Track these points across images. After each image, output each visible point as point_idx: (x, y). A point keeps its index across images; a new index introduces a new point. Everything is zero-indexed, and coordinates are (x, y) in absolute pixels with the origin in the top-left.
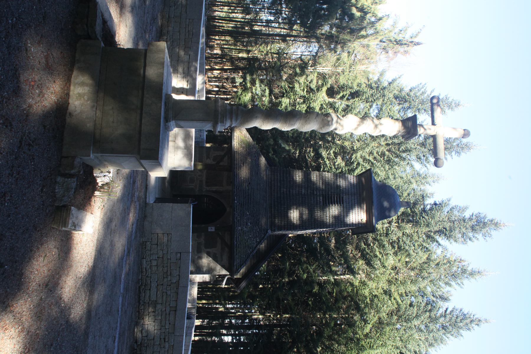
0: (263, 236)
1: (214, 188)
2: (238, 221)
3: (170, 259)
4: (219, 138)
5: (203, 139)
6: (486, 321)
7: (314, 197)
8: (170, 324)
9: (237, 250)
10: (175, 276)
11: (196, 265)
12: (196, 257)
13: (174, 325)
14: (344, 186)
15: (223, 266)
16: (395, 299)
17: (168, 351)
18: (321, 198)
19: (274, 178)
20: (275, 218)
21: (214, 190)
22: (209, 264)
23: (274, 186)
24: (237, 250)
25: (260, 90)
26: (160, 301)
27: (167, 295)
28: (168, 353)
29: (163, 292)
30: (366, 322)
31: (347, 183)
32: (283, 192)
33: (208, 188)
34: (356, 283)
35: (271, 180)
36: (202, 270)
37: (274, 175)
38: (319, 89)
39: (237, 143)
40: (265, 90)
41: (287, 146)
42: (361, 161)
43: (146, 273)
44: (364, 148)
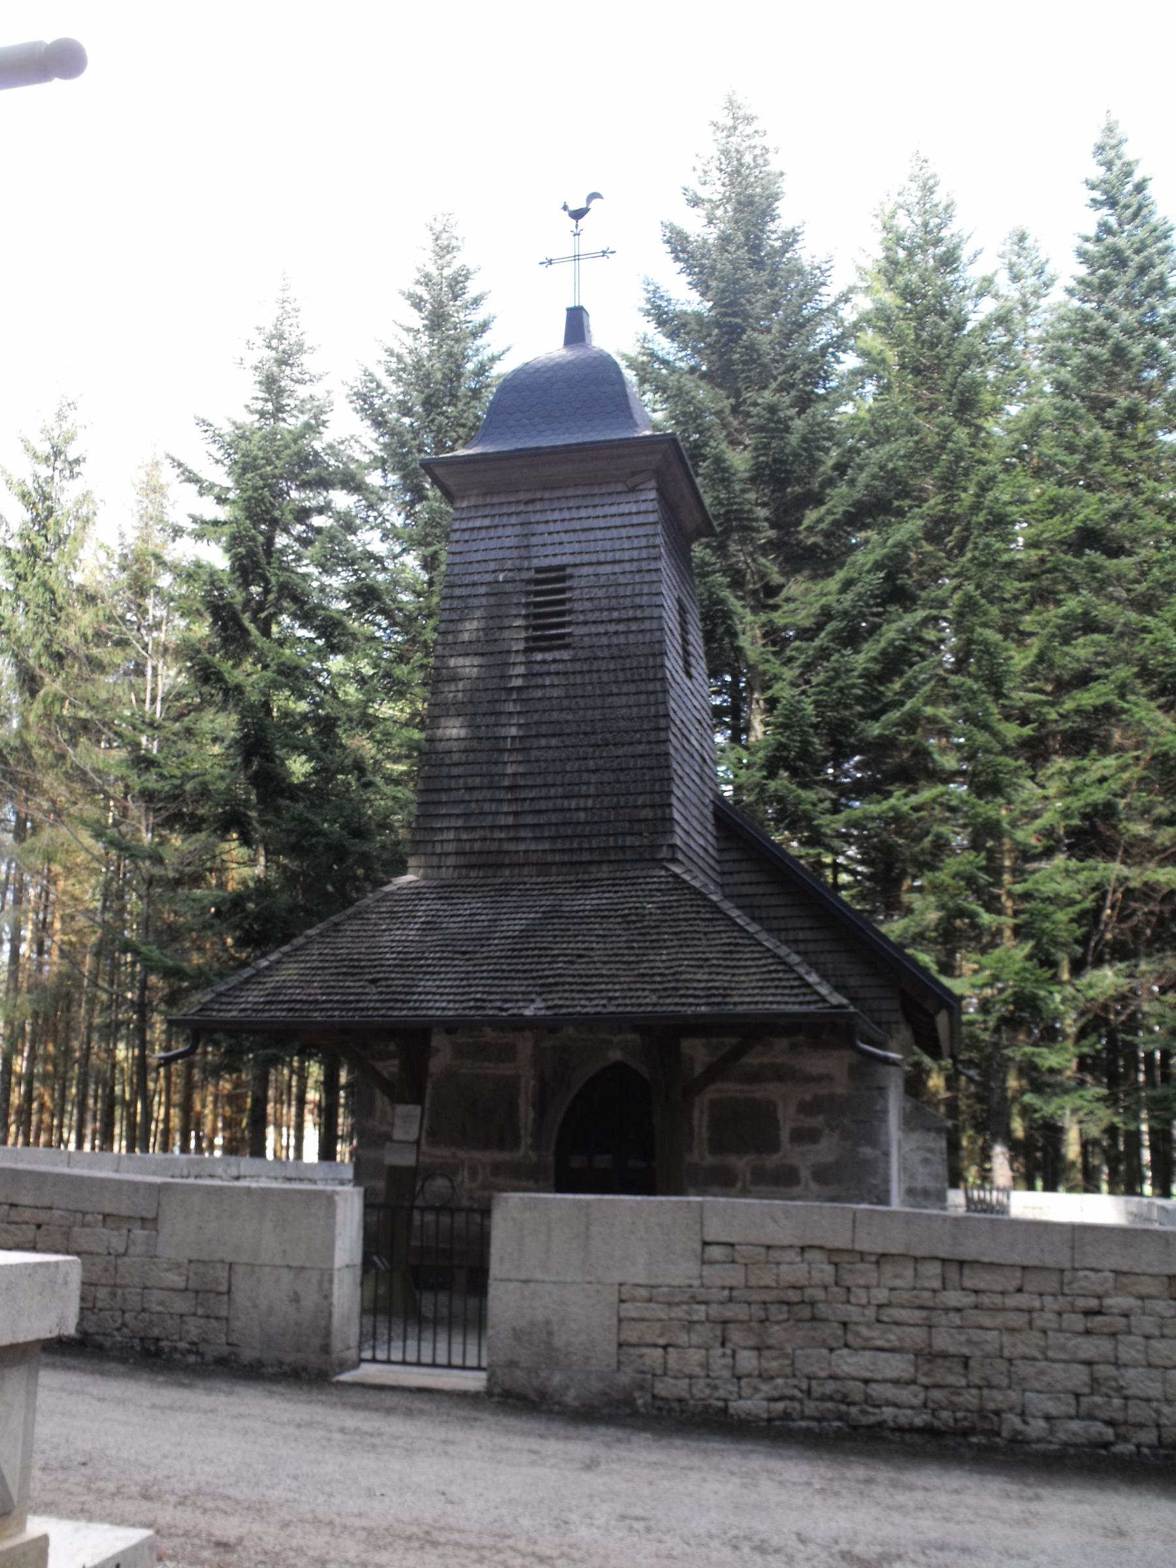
1: (526, 1114)
3: (731, 1289)
8: (1020, 1290)
10: (805, 1266)
13: (1024, 1268)
17: (1141, 1298)
21: (532, 1114)
26: (918, 1336)
27: (889, 1305)
28: (1150, 1297)
29: (879, 1321)
33: (527, 1140)
43: (792, 1398)
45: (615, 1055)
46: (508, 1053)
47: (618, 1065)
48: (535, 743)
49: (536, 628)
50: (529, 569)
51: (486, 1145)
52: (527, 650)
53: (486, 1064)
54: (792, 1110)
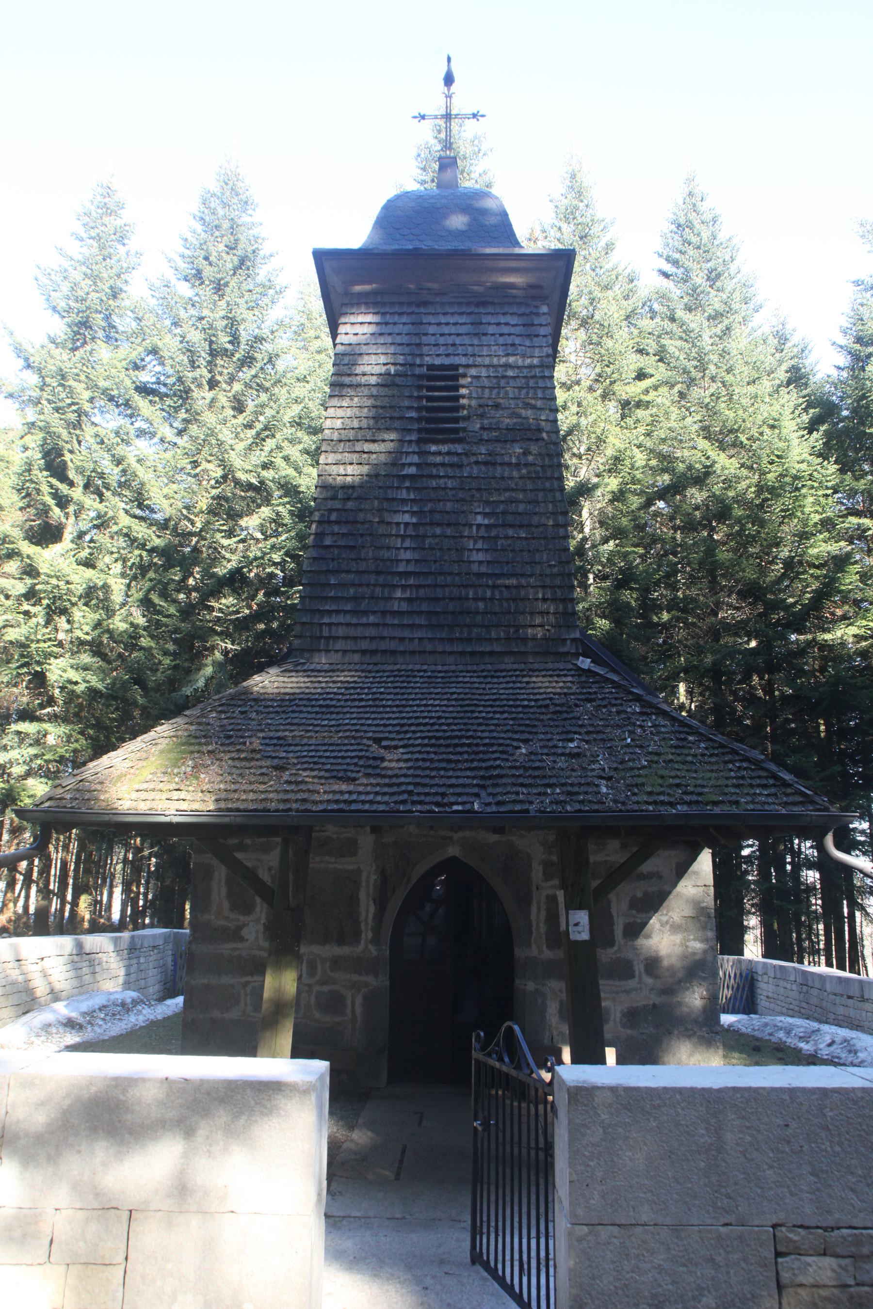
0: (608, 689)
1: (367, 909)
2: (570, 793)
4: (168, 882)
5: (166, 937)
6: (690, 180)
7: (431, 477)
9: (715, 803)
11: (679, 982)
12: (649, 981)
14: (382, 359)
15: (682, 870)
16: (646, 392)
18: (434, 448)
19: (346, 638)
20: (525, 640)
21: (372, 909)
22: (675, 928)
23: (382, 638)
24: (715, 803)
25: (17, 751)
30: (708, 472)
31: (373, 349)
32: (409, 600)
34: (613, 483)
35: (354, 652)
36: (698, 957)
37: (328, 638)
38: (31, 571)
39: (175, 795)
40: (19, 733)
41: (202, 672)
42: (258, 457)
44: (221, 444)
45: (453, 851)
46: (349, 848)
47: (454, 860)
48: (429, 531)
49: (428, 420)
50: (421, 366)
51: (325, 940)
52: (419, 441)
53: (327, 858)
54: (625, 906)
